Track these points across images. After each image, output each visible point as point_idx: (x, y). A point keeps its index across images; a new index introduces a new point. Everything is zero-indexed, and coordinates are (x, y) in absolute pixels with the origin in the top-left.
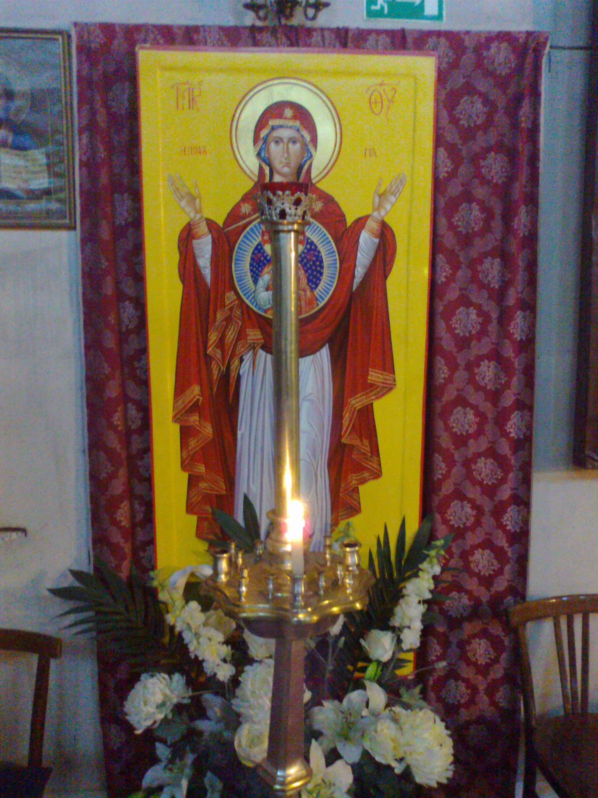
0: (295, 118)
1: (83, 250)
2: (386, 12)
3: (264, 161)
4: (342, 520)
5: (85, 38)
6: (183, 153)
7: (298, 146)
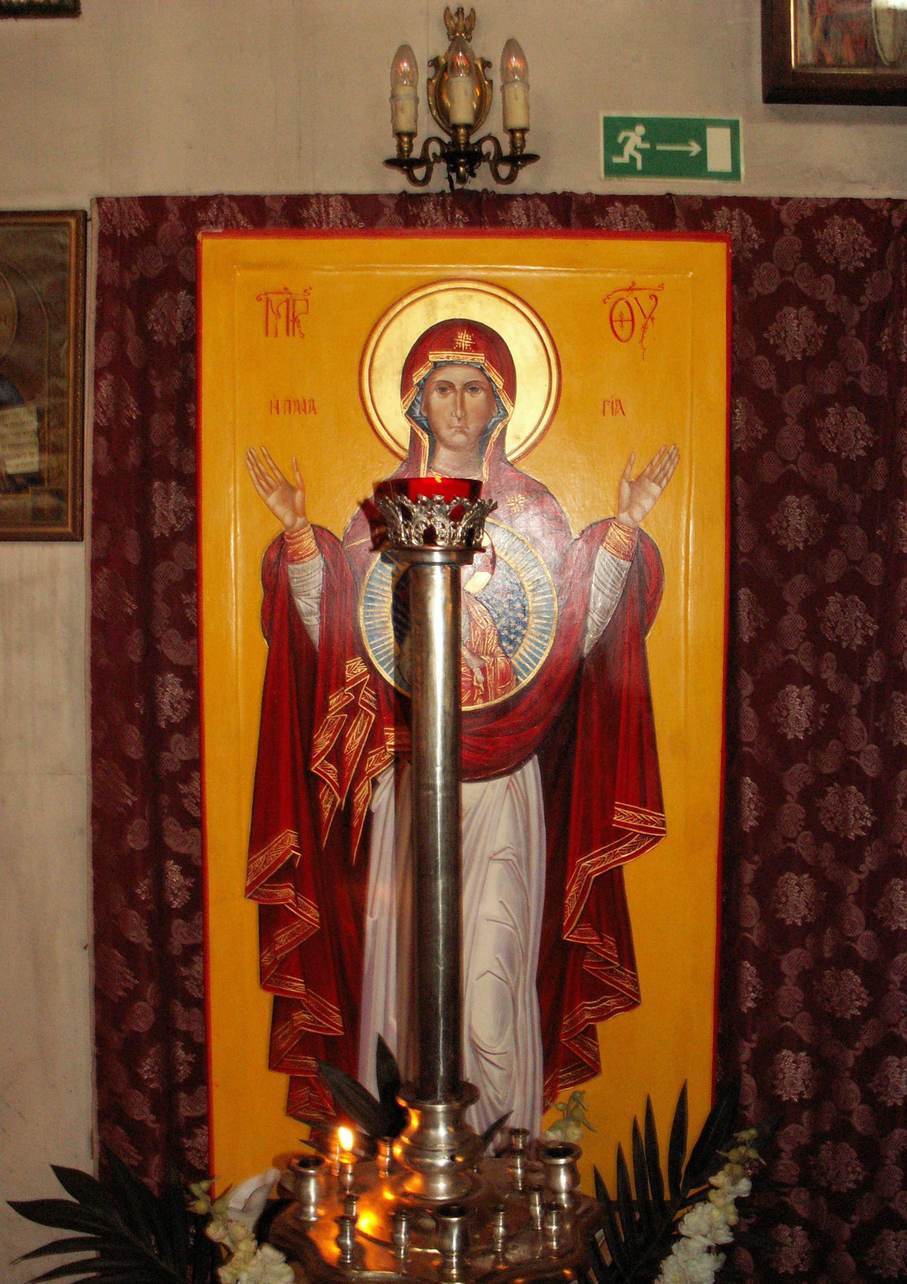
0: (474, 348)
1: (94, 580)
2: (639, 166)
3: (418, 423)
4: (562, 1088)
5: (115, 221)
6: (274, 410)
7: (481, 395)
